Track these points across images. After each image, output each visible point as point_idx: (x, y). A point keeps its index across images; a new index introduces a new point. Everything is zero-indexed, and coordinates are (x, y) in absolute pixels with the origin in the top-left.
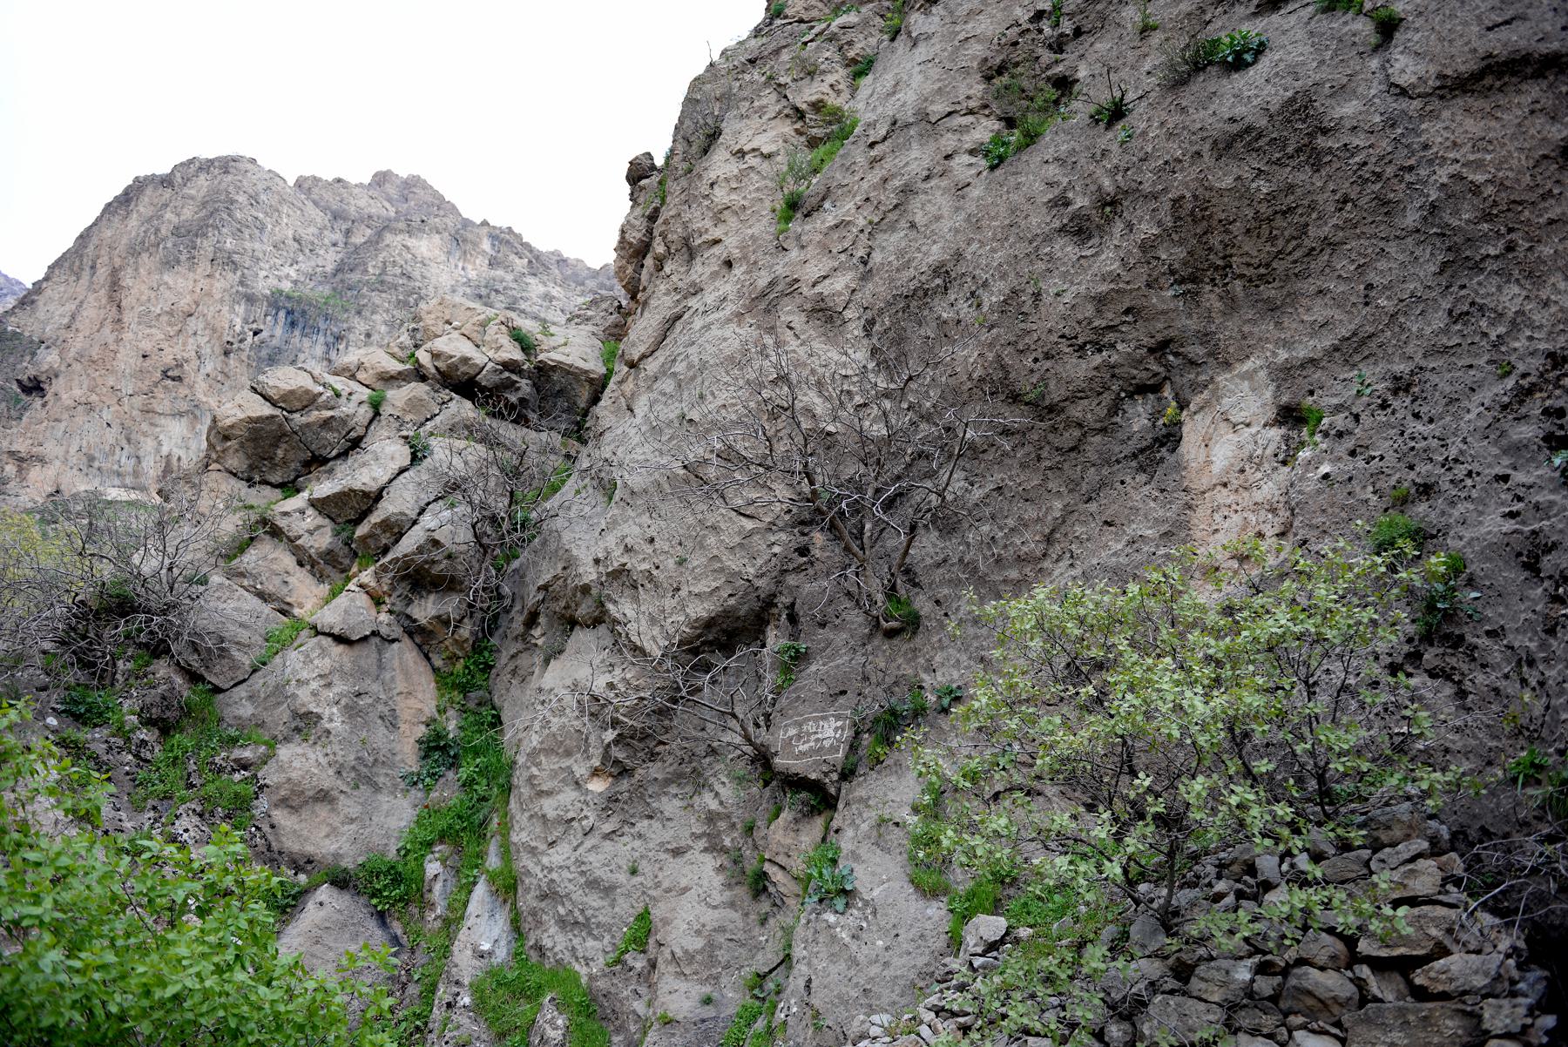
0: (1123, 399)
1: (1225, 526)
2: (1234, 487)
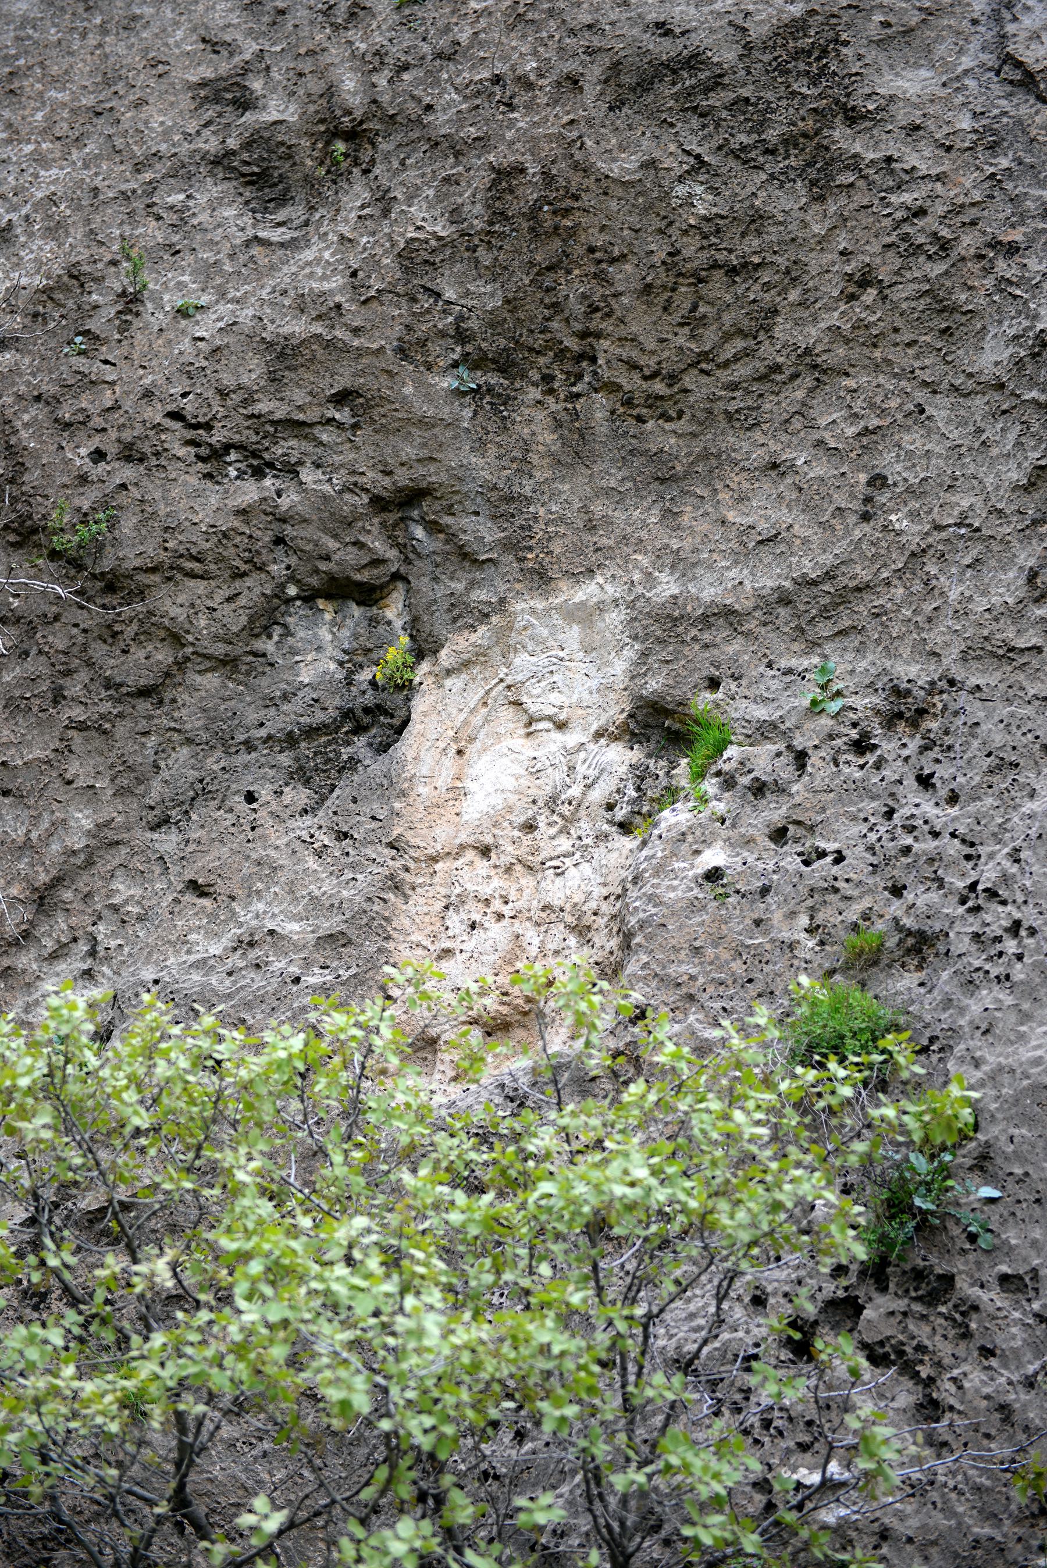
0: (289, 601)
1: (468, 946)
2: (505, 860)
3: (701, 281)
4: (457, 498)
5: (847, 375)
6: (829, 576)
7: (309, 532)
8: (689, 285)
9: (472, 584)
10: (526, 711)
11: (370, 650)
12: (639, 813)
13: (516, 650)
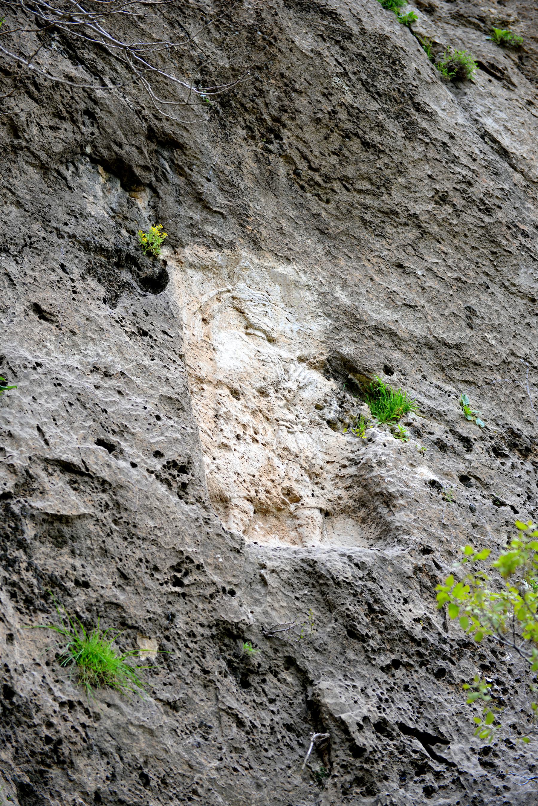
3: (349, 138)
4: (198, 163)
5: (439, 242)
6: (458, 346)
7: (112, 121)
8: (340, 135)
9: (205, 220)
11: (127, 218)
12: (342, 421)
13: (238, 278)
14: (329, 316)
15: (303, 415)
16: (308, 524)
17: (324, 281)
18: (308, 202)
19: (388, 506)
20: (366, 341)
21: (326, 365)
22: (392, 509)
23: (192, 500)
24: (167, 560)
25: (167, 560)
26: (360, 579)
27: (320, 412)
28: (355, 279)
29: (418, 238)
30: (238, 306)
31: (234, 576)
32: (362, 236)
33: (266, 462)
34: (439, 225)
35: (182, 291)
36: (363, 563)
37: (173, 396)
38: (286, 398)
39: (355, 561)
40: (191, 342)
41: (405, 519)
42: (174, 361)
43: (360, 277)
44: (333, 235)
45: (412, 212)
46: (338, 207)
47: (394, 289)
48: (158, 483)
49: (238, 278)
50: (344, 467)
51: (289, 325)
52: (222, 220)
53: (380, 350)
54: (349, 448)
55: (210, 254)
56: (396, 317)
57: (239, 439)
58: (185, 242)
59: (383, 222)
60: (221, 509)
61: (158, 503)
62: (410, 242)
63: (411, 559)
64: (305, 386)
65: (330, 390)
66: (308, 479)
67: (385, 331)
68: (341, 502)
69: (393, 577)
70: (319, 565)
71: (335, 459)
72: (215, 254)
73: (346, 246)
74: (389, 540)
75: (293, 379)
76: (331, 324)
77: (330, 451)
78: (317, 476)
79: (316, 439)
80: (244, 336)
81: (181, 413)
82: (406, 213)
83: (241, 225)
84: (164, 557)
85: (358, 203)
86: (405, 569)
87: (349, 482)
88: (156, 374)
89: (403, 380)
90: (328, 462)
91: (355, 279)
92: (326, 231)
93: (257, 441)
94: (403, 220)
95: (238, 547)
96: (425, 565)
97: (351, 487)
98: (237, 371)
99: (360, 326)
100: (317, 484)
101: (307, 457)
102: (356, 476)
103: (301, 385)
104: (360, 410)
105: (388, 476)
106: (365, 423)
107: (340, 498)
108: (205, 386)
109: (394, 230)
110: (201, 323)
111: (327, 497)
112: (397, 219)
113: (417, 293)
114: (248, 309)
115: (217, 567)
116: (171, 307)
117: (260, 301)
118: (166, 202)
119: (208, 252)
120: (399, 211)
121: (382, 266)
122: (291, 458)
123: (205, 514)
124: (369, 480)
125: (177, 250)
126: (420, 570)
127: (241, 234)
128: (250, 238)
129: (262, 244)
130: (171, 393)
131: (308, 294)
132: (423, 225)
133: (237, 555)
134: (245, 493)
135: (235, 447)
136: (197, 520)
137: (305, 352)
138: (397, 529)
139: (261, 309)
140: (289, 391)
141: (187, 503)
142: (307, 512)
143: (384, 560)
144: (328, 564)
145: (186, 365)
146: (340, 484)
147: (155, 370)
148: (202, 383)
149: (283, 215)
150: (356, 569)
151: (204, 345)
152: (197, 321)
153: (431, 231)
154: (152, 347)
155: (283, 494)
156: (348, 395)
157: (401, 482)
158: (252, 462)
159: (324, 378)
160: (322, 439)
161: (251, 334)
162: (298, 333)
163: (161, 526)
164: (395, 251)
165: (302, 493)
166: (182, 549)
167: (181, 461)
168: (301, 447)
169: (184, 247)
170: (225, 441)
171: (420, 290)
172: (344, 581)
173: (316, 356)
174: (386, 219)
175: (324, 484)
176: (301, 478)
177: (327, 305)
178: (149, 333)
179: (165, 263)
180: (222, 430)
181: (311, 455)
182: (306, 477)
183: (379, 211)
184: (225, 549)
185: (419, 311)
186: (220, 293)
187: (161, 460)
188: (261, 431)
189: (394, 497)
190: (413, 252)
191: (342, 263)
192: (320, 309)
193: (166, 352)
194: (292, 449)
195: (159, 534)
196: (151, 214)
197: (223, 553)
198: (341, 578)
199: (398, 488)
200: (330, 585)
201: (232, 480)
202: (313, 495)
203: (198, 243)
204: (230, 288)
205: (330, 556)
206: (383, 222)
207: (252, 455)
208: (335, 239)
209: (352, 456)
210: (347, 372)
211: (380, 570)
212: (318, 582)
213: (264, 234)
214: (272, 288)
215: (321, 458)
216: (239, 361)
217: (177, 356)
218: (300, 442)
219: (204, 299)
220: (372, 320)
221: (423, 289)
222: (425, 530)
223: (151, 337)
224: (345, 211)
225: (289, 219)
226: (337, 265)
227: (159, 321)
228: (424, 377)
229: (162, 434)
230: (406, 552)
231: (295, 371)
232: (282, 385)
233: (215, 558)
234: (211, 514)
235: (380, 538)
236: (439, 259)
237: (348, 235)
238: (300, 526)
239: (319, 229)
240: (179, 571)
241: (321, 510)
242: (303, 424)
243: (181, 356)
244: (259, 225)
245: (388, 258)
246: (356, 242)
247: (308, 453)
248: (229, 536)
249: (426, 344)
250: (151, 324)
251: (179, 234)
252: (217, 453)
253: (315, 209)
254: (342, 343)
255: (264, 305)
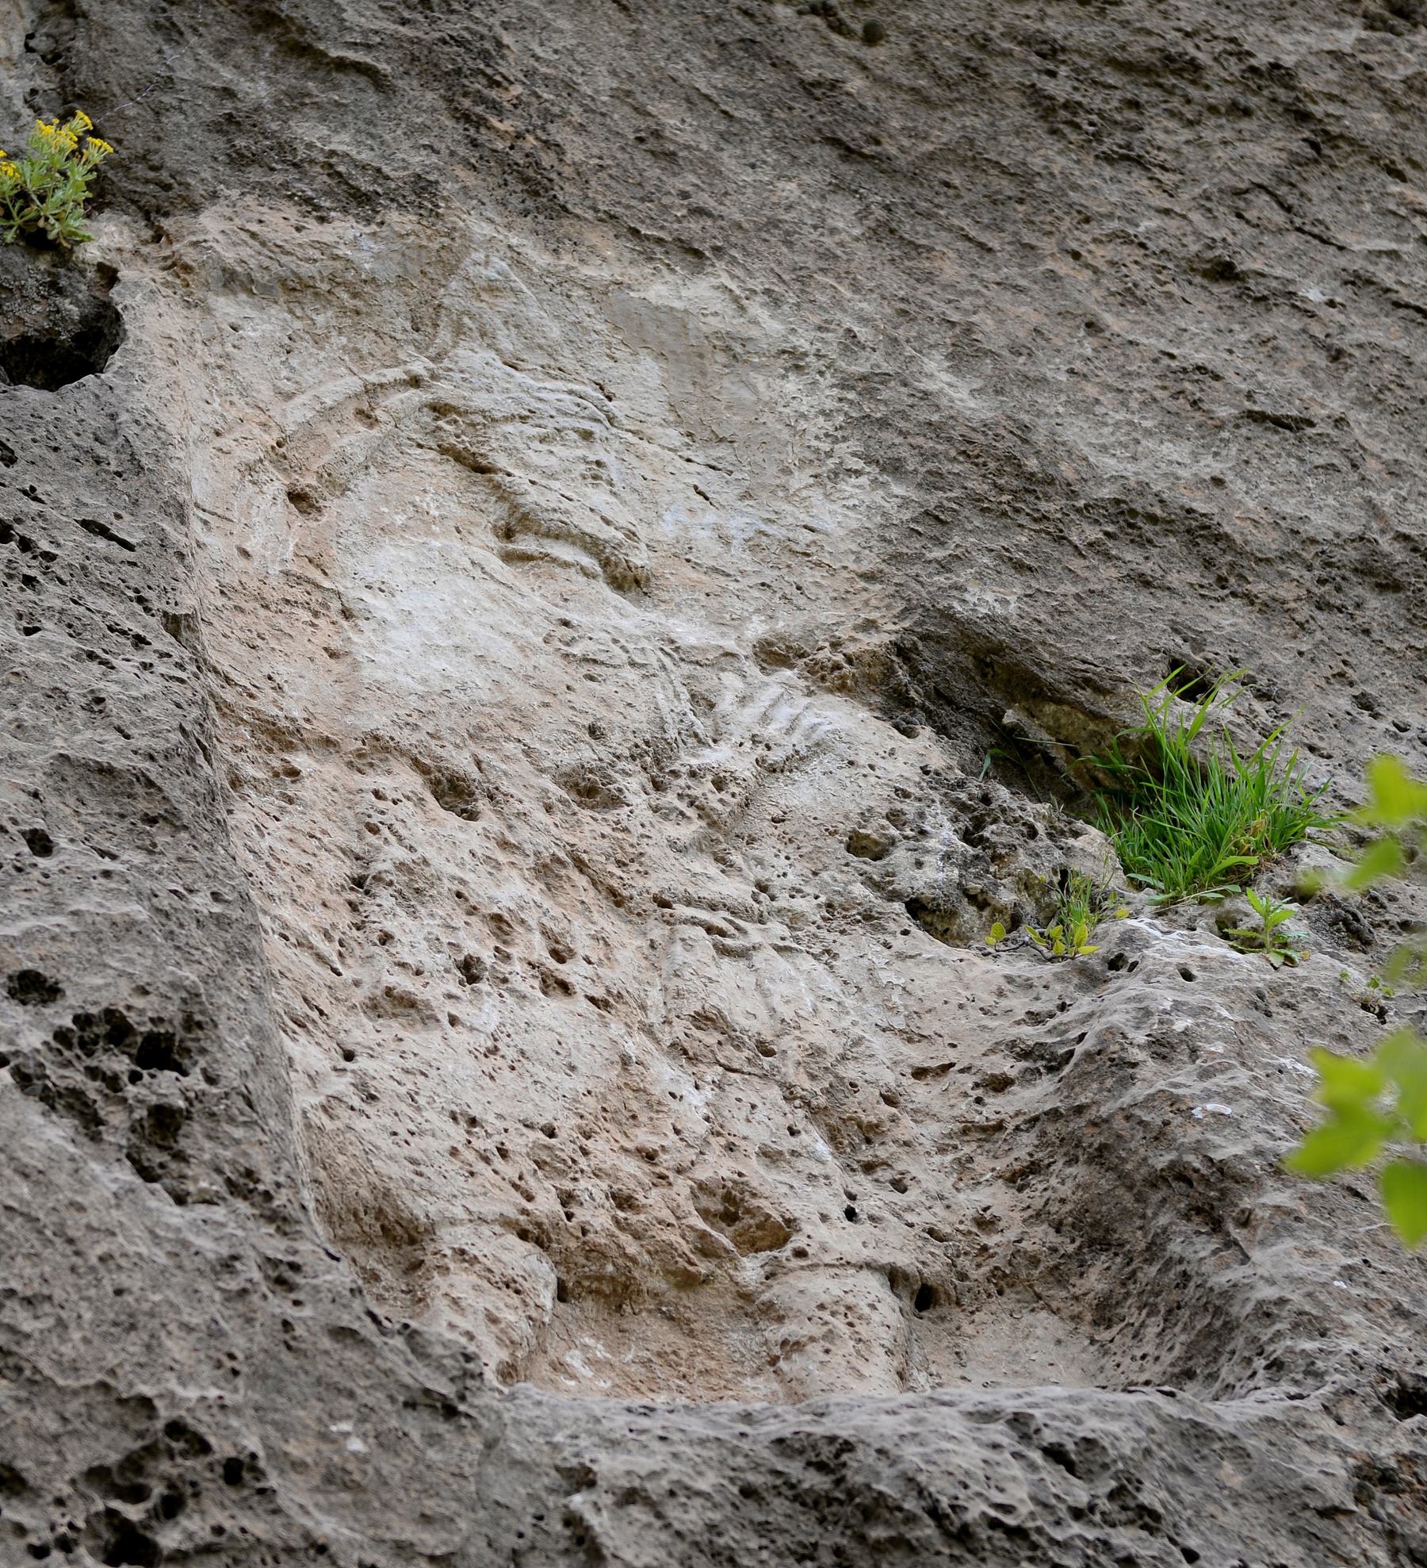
5: (1400, 176)
9: (295, 102)
10: (502, 493)
12: (980, 901)
13: (459, 330)
14: (895, 468)
15: (792, 879)
16: (830, 1335)
17: (863, 333)
18: (781, 35)
19: (1217, 1226)
20: (1076, 564)
21: (890, 671)
22: (1236, 1233)
23: (208, 1183)
24: (69, 1444)
25: (69, 1444)
26: (1077, 1514)
27: (874, 869)
28: (1010, 326)
29: (1296, 161)
30: (465, 442)
31: (426, 1519)
32: (1036, 163)
33: (613, 1074)
34: (1394, 107)
35: (189, 375)
36: (1089, 1443)
37: (120, 764)
38: (703, 812)
39: (1049, 1437)
40: (227, 579)
41: (1300, 1267)
42: (140, 641)
43: (1035, 319)
44: (902, 162)
45: (1262, 60)
46: (920, 56)
47: (1200, 358)
48: (32, 1111)
49: (459, 330)
50: (1000, 1084)
51: (711, 517)
52: (372, 97)
53: (1144, 598)
54: (1020, 1004)
55: (316, 231)
56: (1210, 466)
57: (473, 979)
58: (199, 190)
59: (1134, 105)
60: (388, 1276)
61: (24, 1189)
62: (1263, 179)
63: (1342, 1436)
64: (796, 761)
65: (915, 775)
66: (823, 1148)
67: (1167, 525)
68: (991, 1240)
69: (1248, 1508)
70: (865, 1456)
71: (951, 1055)
72: (343, 230)
73: (967, 209)
74: (1228, 1371)
75: (737, 734)
76: (905, 502)
77: (929, 1026)
78: (870, 1133)
79: (860, 978)
80: (495, 564)
81: (162, 837)
82: (1235, 67)
83: (466, 117)
84: (53, 1425)
85: (1010, 33)
86: (1311, 1474)
87: (1025, 1146)
88: (43, 680)
89: (1265, 718)
90: (920, 1073)
91: (1010, 326)
92: (868, 150)
93: (565, 988)
94: (1220, 95)
95: (447, 1389)
96: (1409, 1459)
97: (1034, 1168)
98: (462, 698)
99: (1044, 506)
100: (869, 1168)
101: (816, 1052)
102: (1054, 1114)
103: (775, 756)
104: (1068, 851)
105: (1209, 1096)
106: (1094, 906)
107: (985, 1223)
108: (300, 760)
109: (1187, 134)
110: (283, 509)
111: (923, 1218)
112: (1195, 93)
113: (1307, 371)
114: (509, 452)
115: (335, 1479)
116: (131, 431)
117: (564, 422)
118: (106, 31)
119: (311, 224)
120: (1203, 58)
121: (1136, 274)
122: (738, 1058)
123: (276, 1247)
124: (1119, 1124)
125: (166, 223)
126: (1387, 1479)
127: (462, 151)
128: (509, 167)
129: (568, 194)
130: (111, 750)
131: (792, 385)
132: (1318, 110)
133: (442, 1427)
134: (508, 1204)
135: (451, 1008)
136: (228, 1264)
137: (788, 624)
138: (1265, 1313)
139: (572, 451)
140: (719, 784)
141: (180, 1200)
142: (822, 1286)
143: (1197, 1434)
144: (911, 1454)
145: (201, 664)
146: (983, 1164)
147: (38, 665)
148: (289, 747)
149: (663, 84)
150: (1054, 1477)
151: (298, 593)
152: (263, 502)
153: (1358, 130)
154: (29, 581)
155: (705, 1214)
156: (1002, 794)
157: (1270, 1116)
158: (542, 1074)
159: (886, 728)
160: (885, 976)
161: (526, 558)
162: (753, 547)
163: (37, 1287)
164: (1196, 217)
165: (794, 1207)
166: (147, 1390)
167: (142, 1014)
168: (787, 1012)
169: (195, 209)
170: (404, 983)
171: (1320, 359)
172: (994, 1524)
173: (842, 633)
174: (1146, 95)
175: (905, 1163)
176: (787, 1143)
177: (884, 423)
178: (19, 529)
179: (109, 275)
180: (386, 938)
181: (835, 1046)
182: (815, 1141)
183: (1113, 63)
184: (377, 1398)
185: (1321, 440)
186: (372, 391)
187: (48, 1011)
188: (582, 945)
189: (1240, 1179)
190: (1279, 217)
191: (950, 270)
192: (854, 445)
193: (104, 603)
194: (740, 1020)
195: (27, 1325)
196: (39, 83)
197: (365, 1414)
198: (975, 1510)
199: (1261, 1140)
200: (925, 1545)
201: (437, 1146)
202: (851, 1214)
203: (263, 191)
204: (419, 367)
205: (920, 1421)
206: (1134, 105)
207: (541, 1042)
208: (912, 178)
209: (1031, 1034)
210: (994, 698)
211: (1179, 1480)
212: (861, 1538)
213: (575, 152)
214: (623, 369)
215: (883, 1055)
216: (468, 661)
217: (155, 622)
218: (780, 989)
219: (295, 414)
220: (1100, 482)
221: (1337, 355)
222: (1400, 1312)
223: (26, 545)
224: (954, 70)
225: (693, 99)
226: (929, 278)
227: (68, 482)
228: (1365, 703)
229: (56, 906)
230: (1313, 1403)
231: (743, 700)
232: (686, 760)
233: (324, 1436)
234: (303, 1246)
235: (1190, 1375)
236: (1399, 239)
237: (976, 162)
238: (792, 1346)
239: (835, 142)
240: (136, 1494)
241: (894, 1277)
242: (794, 920)
243: (175, 624)
244: (548, 116)
245: (1163, 243)
246: (1008, 188)
247: (819, 1036)
248: (398, 1342)
249: (1364, 571)
250: (31, 493)
251: (172, 155)
252: (361, 1031)
253: (815, 65)
254: (963, 575)
255: (587, 435)
